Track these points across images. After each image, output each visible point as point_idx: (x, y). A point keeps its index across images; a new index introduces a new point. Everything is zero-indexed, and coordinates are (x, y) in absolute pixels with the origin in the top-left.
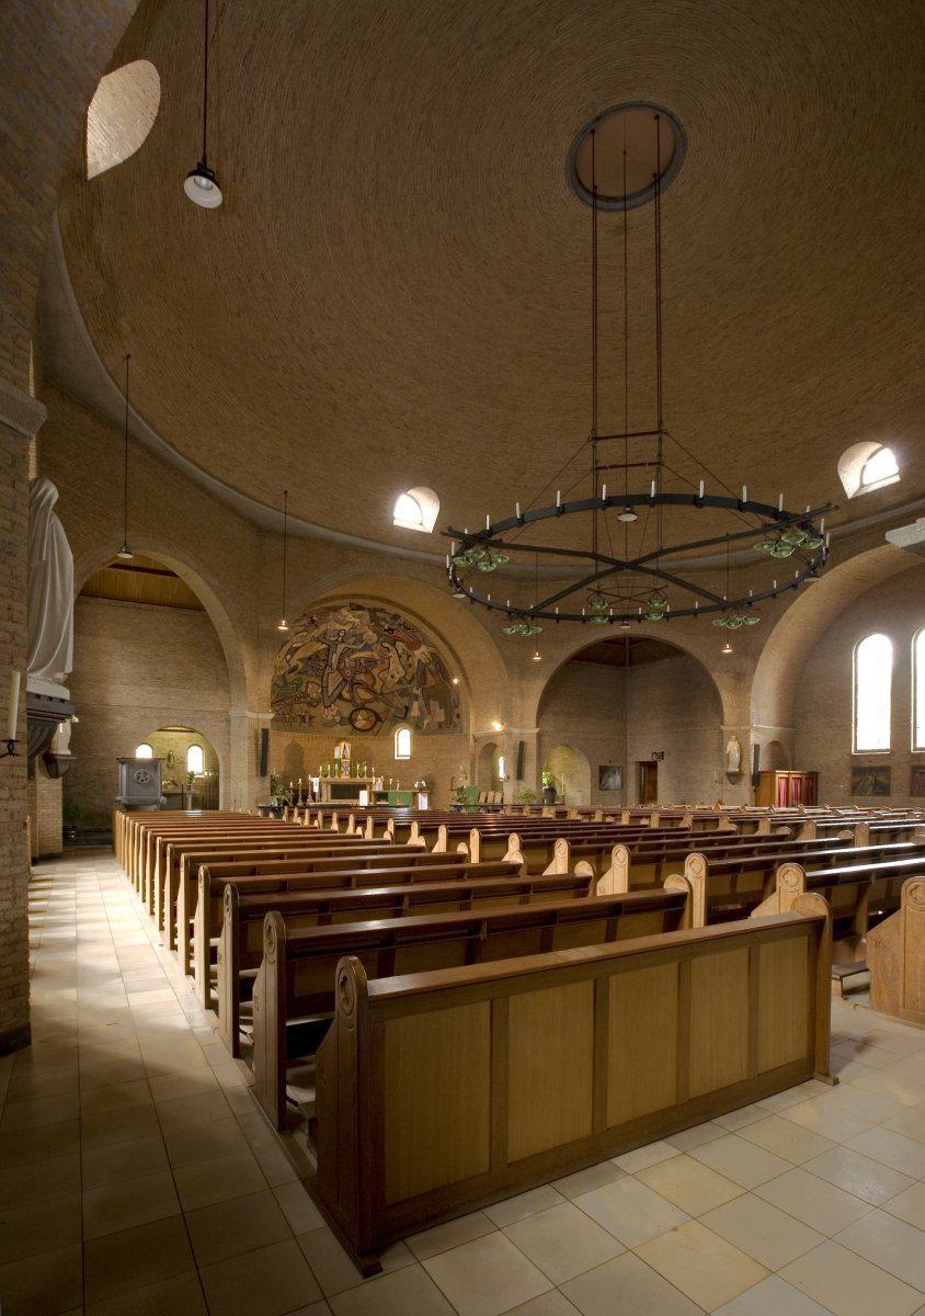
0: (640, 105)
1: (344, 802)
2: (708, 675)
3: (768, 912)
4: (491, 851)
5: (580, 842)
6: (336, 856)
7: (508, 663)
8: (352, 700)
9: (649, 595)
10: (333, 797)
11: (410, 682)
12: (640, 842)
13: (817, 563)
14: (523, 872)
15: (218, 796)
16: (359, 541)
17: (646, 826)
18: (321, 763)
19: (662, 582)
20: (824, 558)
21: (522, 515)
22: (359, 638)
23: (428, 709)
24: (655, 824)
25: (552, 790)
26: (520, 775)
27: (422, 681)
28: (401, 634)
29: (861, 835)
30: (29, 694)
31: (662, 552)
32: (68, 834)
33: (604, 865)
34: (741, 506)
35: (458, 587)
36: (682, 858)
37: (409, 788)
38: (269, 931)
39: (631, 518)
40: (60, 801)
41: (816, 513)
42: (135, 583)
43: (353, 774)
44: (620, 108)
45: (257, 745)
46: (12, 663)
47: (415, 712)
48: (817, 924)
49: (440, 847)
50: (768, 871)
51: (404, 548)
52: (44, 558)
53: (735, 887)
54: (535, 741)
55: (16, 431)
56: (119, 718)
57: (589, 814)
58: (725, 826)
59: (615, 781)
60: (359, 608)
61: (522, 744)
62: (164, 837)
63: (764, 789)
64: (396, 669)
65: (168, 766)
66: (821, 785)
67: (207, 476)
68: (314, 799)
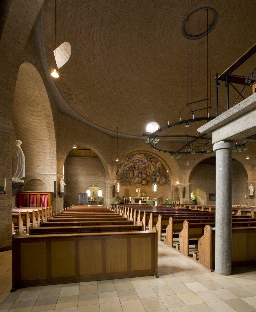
0: (201, 8)
6: (109, 217)
8: (141, 177)
10: (135, 202)
11: (156, 172)
15: (103, 202)
16: (138, 137)
17: (208, 212)
18: (132, 194)
22: (142, 161)
23: (161, 179)
26: (184, 196)
27: (159, 171)
28: (153, 160)
39: (189, 126)
42: (83, 153)
43: (141, 196)
44: (195, 11)
45: (112, 189)
47: (158, 180)
54: (188, 187)
56: (80, 184)
60: (141, 154)
61: (184, 188)
64: (153, 169)
68: (130, 203)
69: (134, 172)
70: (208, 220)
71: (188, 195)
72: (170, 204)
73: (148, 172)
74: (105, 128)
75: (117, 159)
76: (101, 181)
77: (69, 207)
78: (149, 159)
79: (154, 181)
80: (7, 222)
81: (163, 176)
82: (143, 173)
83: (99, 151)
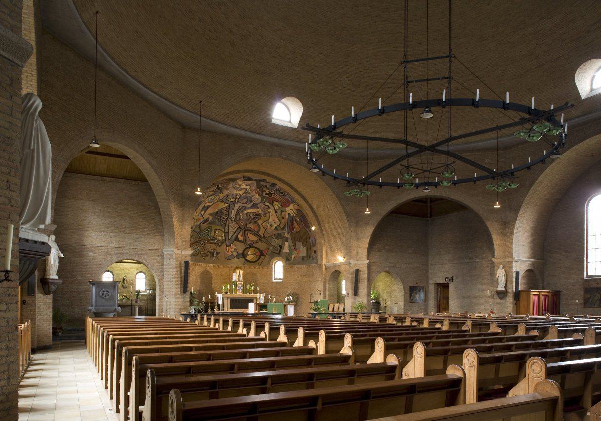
1: (239, 311)
2: (483, 223)
3: (521, 393)
4: (332, 346)
5: (393, 340)
7: (348, 215)
8: (244, 242)
9: (442, 169)
10: (231, 308)
11: (283, 229)
12: (434, 340)
13: (559, 145)
14: (351, 361)
18: (224, 283)
19: (451, 159)
20: (564, 141)
21: (356, 115)
22: (250, 200)
24: (446, 327)
25: (377, 303)
26: (356, 293)
27: (292, 228)
28: (278, 197)
29: (590, 336)
30: (20, 239)
31: (451, 139)
32: (56, 333)
33: (408, 356)
34: (505, 106)
35: (314, 164)
36: (461, 352)
37: (282, 302)
38: (172, 403)
39: (430, 115)
40: (51, 310)
41: (558, 109)
42: (102, 164)
43: (245, 292)
45: (181, 272)
46: (9, 218)
47: (286, 249)
48: (553, 402)
49: (299, 343)
50: (521, 361)
51: (279, 138)
52: (32, 148)
53: (498, 374)
55: (13, 62)
56: (91, 254)
57: (401, 320)
58: (494, 329)
59: (420, 296)
60: (250, 179)
61: (357, 271)
62: (114, 335)
63: (523, 303)
65: (123, 287)
66: (563, 301)
67: (150, 92)
69: (227, 227)
70: (396, 345)
71: (365, 291)
72: (323, 312)
73: (261, 227)
74: (166, 99)
75: (199, 189)
76: (152, 248)
77: (26, 323)
78: (267, 194)
79: (278, 252)
80: (4, 382)
81: (300, 242)
82: (249, 230)
83: (150, 163)
